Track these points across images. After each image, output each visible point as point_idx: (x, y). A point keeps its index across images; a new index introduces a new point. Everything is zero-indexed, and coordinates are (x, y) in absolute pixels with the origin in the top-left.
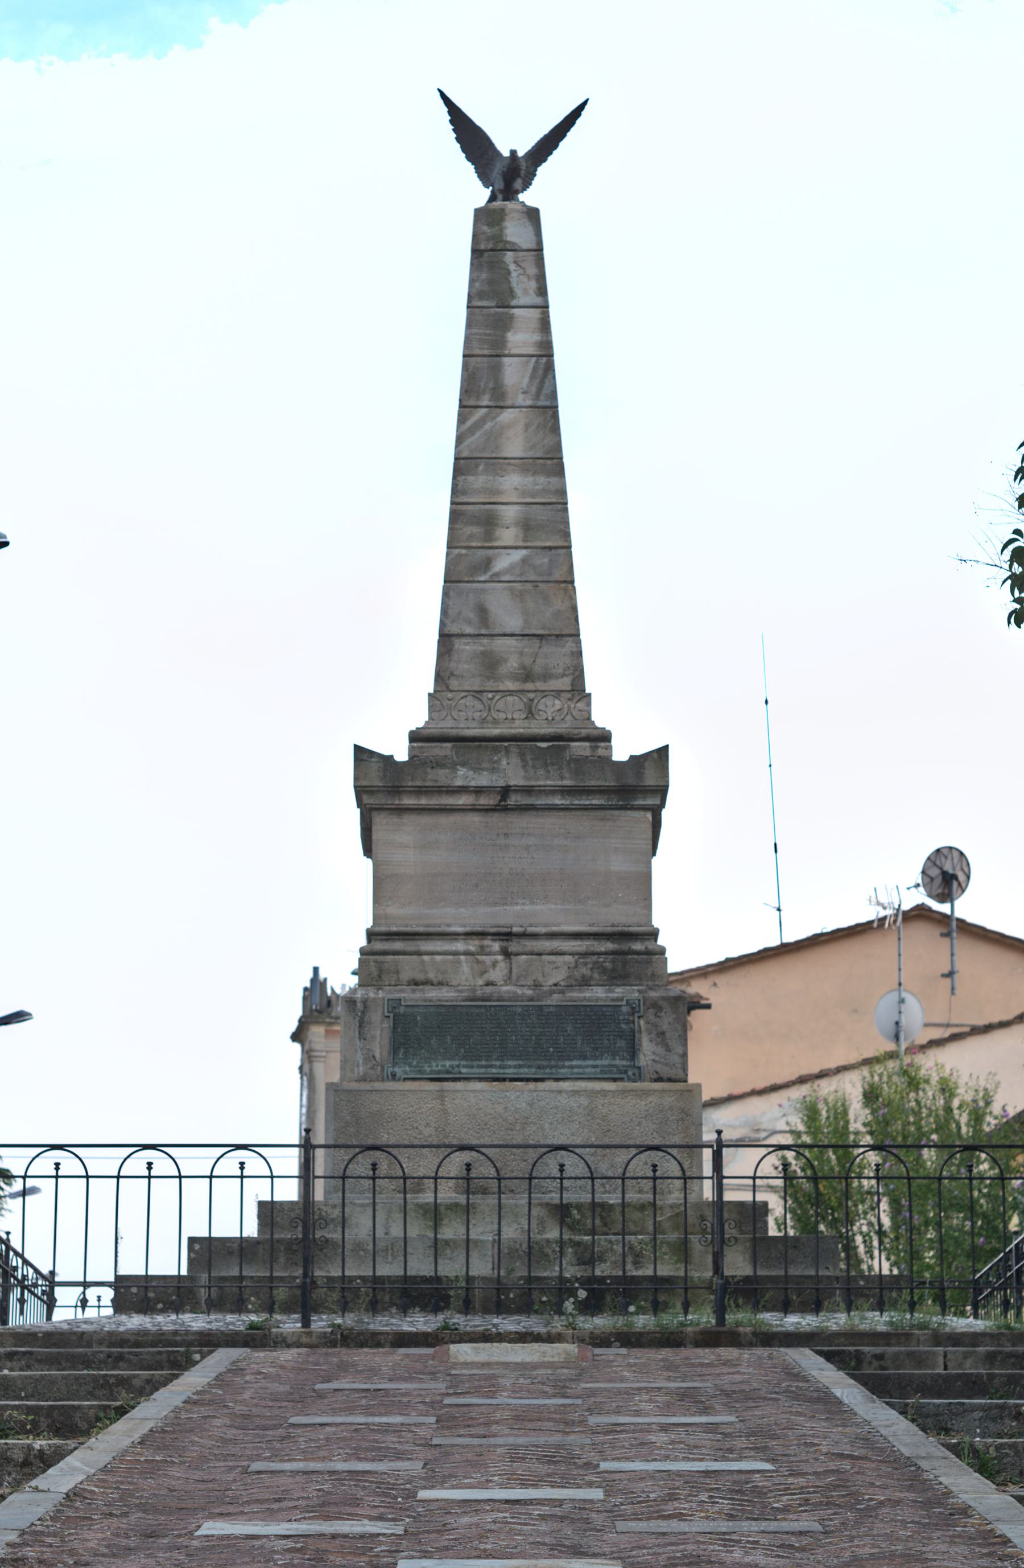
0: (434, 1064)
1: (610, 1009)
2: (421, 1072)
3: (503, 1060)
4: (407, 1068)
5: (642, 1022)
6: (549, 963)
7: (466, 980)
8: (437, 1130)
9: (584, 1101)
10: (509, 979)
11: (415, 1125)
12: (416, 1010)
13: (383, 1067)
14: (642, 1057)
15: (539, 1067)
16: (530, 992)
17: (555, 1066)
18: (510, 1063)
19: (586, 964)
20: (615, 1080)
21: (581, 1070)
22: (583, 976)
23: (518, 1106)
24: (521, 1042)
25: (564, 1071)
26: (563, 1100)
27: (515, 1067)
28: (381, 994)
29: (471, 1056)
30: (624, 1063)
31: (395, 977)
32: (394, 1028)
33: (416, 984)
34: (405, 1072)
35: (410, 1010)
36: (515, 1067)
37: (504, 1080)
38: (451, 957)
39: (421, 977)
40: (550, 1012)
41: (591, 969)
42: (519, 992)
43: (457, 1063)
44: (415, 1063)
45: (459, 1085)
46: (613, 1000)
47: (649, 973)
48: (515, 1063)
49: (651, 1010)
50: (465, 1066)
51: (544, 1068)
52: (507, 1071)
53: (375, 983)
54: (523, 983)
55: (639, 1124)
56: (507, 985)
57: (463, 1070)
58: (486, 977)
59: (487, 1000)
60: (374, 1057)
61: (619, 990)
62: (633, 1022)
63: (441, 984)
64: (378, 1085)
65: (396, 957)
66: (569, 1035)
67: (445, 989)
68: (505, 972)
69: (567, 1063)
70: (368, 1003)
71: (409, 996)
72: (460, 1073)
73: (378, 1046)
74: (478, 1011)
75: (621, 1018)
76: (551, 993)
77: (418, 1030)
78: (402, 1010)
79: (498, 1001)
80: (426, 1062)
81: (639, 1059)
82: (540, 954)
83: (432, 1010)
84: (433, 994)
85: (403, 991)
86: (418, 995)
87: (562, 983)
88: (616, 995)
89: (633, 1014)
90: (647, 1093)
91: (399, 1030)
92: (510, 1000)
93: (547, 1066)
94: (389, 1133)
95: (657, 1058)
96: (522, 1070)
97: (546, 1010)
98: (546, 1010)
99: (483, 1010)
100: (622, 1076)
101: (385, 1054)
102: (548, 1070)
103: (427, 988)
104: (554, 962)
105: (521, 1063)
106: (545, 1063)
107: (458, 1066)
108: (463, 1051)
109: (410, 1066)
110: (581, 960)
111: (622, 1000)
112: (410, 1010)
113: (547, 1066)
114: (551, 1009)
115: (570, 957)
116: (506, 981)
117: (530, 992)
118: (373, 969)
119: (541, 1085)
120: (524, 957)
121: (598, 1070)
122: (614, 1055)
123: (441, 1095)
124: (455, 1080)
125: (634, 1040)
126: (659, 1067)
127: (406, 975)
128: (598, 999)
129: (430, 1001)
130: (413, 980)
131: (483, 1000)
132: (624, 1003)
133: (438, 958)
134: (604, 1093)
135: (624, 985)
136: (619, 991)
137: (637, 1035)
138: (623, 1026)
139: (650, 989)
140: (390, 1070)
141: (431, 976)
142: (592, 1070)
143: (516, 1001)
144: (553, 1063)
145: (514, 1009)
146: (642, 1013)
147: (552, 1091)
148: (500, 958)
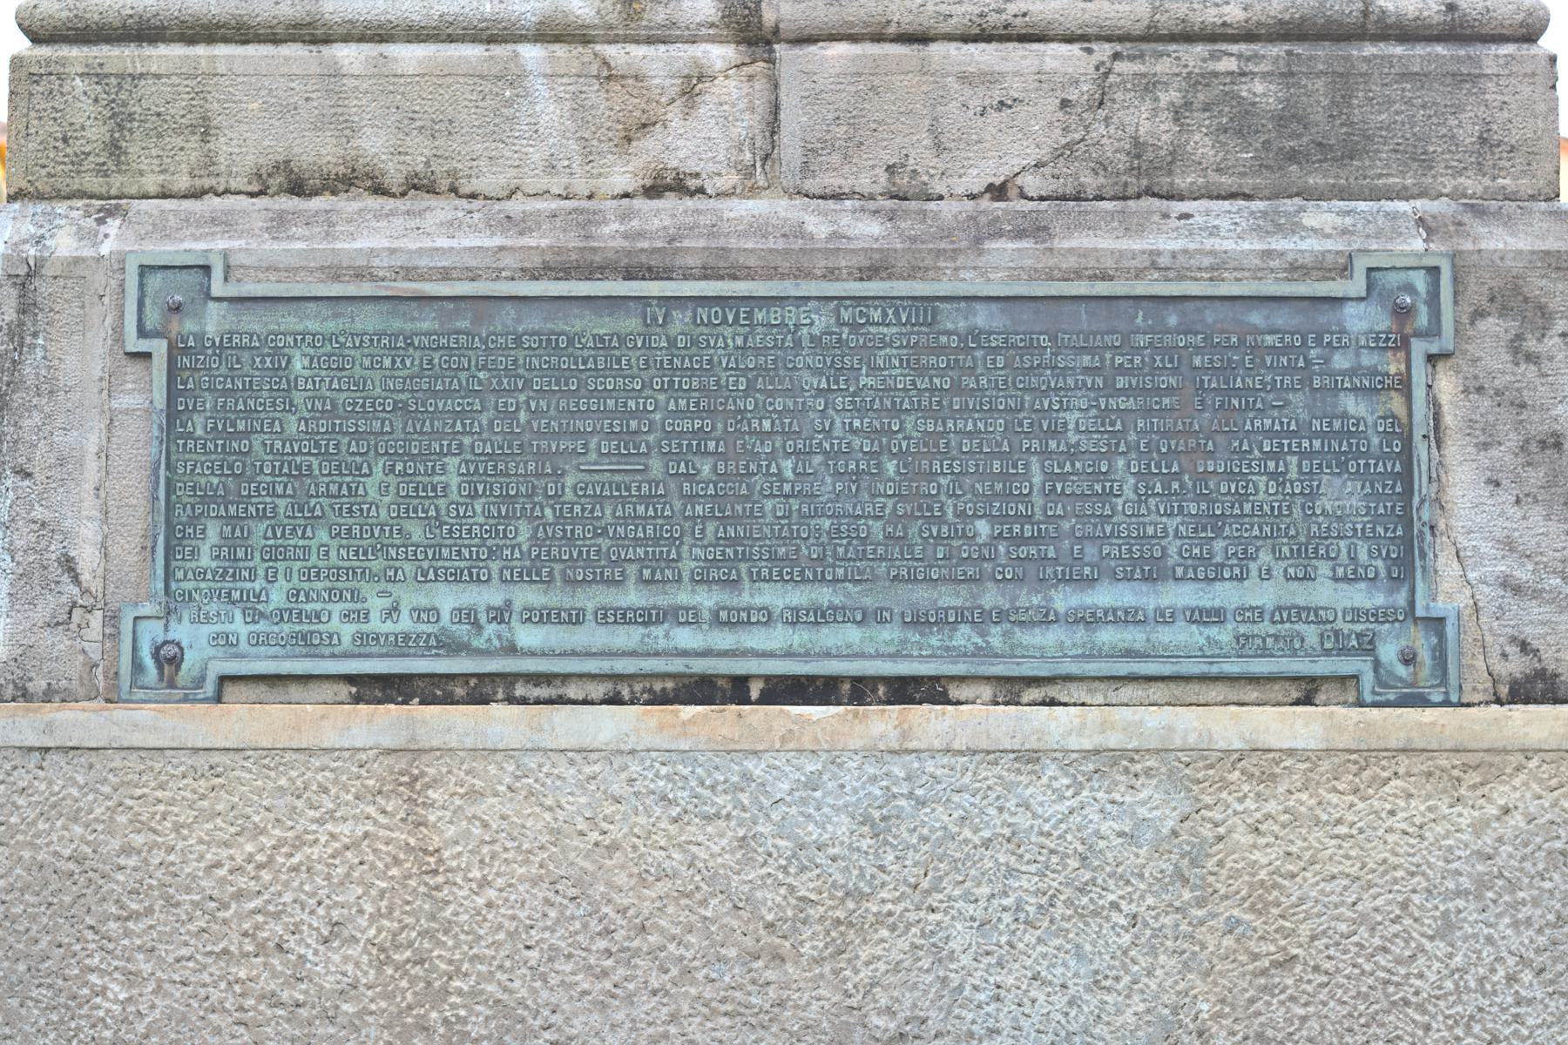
0: (376, 604)
1: (1283, 318)
2: (306, 643)
3: (733, 584)
4: (239, 627)
5: (1447, 385)
6: (963, 78)
7: (551, 168)
8: (382, 955)
9: (1155, 804)
10: (762, 162)
11: (274, 930)
12: (288, 321)
13: (113, 619)
14: (1447, 567)
15: (918, 621)
16: (868, 230)
17: (1001, 616)
18: (775, 597)
19: (1148, 86)
20: (1308, 691)
21: (1133, 637)
22: (1138, 148)
23: (813, 833)
24: (827, 486)
25: (1049, 638)
26: (1044, 799)
27: (795, 618)
28: (113, 238)
29: (570, 558)
30: (1360, 597)
31: (193, 151)
32: (173, 416)
33: (297, 188)
34: (226, 642)
35: (254, 322)
36: (795, 618)
37: (736, 690)
38: (472, 52)
39: (320, 152)
40: (975, 334)
41: (1178, 113)
42: (817, 225)
43: (492, 596)
44: (277, 597)
45: (500, 722)
46: (1296, 270)
47: (1468, 134)
48: (798, 597)
49: (1491, 324)
50: (543, 617)
51: (943, 621)
52: (755, 639)
53: (92, 182)
54: (832, 181)
55: (1447, 927)
56: (753, 191)
57: (528, 636)
58: (649, 151)
59: (652, 274)
60: (69, 565)
61: (1321, 216)
62: (1404, 386)
63: (420, 185)
64: (79, 722)
65: (201, 50)
66: (1073, 453)
67: (442, 209)
68: (749, 124)
69: (1064, 600)
70: (43, 287)
71: (255, 244)
72: (512, 650)
73: (90, 506)
74: (604, 326)
75: (1340, 362)
76: (981, 234)
77: (293, 426)
78: (213, 321)
79: (707, 274)
80: (335, 595)
81: (1431, 574)
82: (920, 38)
83: (368, 320)
84: (373, 235)
85: (223, 223)
86: (297, 245)
87: (1032, 183)
88: (1312, 244)
89: (1404, 345)
90: (1488, 763)
91: (198, 425)
92: (773, 273)
93: (962, 616)
94: (131, 978)
95: (1523, 574)
96: (830, 637)
97: (953, 321)
98: (953, 321)
99: (632, 324)
100: (1346, 666)
101: (127, 549)
102: (964, 636)
103: (347, 204)
104: (989, 78)
105: (825, 596)
106: (949, 598)
107: (500, 614)
108: (524, 532)
109: (255, 616)
110: (1122, 67)
111: (1345, 270)
112: (254, 322)
113: (962, 616)
114: (982, 317)
115: (1075, 49)
116: (748, 172)
117: (868, 230)
118: (84, 111)
119: (928, 721)
120: (842, 48)
121: (1224, 635)
122: (1304, 557)
123: (409, 773)
124: (480, 690)
125: (1407, 476)
126: (1532, 619)
127: (245, 145)
128: (1219, 266)
129: (359, 275)
130: (284, 167)
131: (629, 276)
132: (1356, 285)
133: (408, 56)
134: (1262, 764)
135: (1345, 194)
136: (1322, 226)
137: (1421, 449)
138: (1353, 405)
139: (1478, 212)
140: (151, 632)
141: (374, 145)
142: (1195, 636)
143: (802, 274)
144: (991, 598)
145: (791, 315)
146: (1447, 341)
147: (992, 754)
148: (720, 54)
